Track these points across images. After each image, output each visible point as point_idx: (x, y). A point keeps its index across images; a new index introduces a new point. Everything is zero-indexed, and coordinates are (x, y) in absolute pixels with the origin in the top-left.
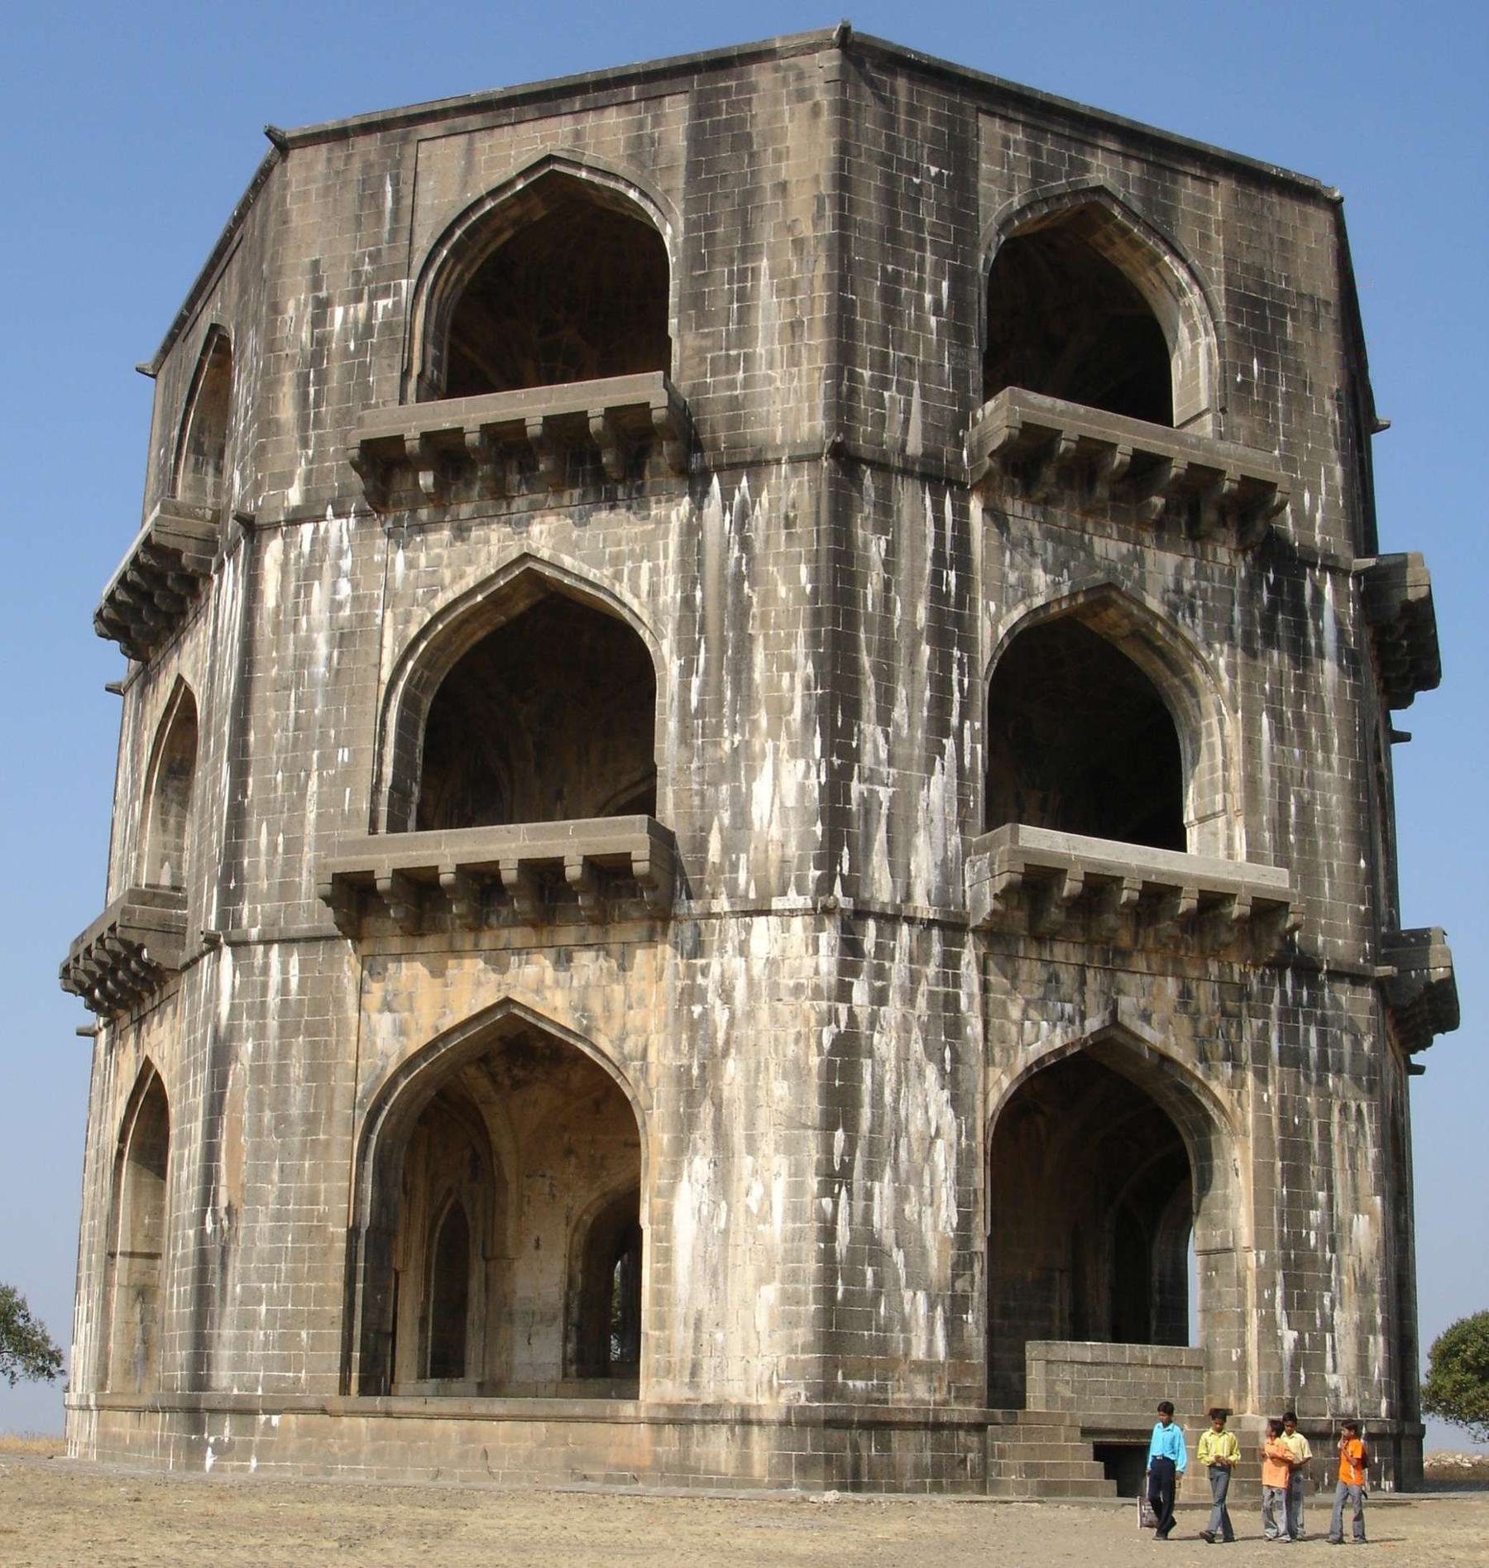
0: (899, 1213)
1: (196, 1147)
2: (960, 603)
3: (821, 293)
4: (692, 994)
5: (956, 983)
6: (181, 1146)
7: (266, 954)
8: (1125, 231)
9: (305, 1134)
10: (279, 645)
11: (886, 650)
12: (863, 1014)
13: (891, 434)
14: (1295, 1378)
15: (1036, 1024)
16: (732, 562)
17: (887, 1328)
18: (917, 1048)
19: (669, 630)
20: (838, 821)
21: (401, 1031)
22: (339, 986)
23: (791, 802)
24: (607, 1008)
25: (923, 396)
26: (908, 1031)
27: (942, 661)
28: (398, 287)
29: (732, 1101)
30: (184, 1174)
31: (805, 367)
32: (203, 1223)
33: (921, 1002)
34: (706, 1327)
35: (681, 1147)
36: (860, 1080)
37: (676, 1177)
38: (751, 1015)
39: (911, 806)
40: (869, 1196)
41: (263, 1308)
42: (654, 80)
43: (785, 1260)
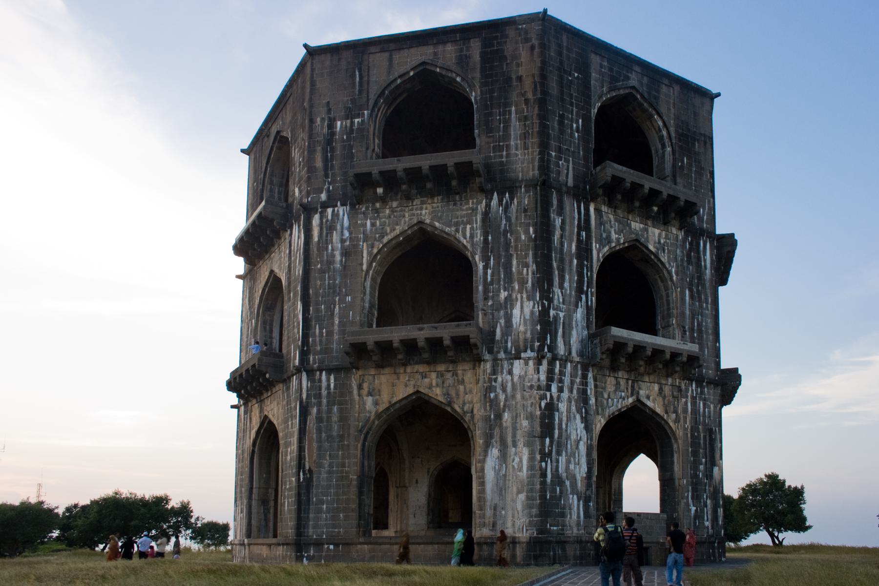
0: (567, 468)
1: (295, 447)
2: (587, 244)
3: (536, 121)
4: (490, 389)
5: (587, 385)
6: (287, 447)
7: (321, 375)
8: (641, 105)
9: (339, 442)
10: (320, 255)
11: (561, 261)
12: (555, 395)
13: (562, 178)
14: (695, 523)
15: (613, 400)
16: (503, 226)
17: (564, 508)
18: (574, 408)
20: (546, 325)
21: (376, 403)
22: (351, 387)
23: (528, 317)
24: (458, 395)
25: (573, 164)
26: (571, 402)
27: (580, 266)
28: (363, 114)
29: (506, 428)
30: (289, 458)
31: (530, 150)
32: (299, 475)
33: (575, 391)
34: (498, 509)
35: (487, 445)
36: (554, 420)
37: (486, 456)
38: (513, 397)
39: (571, 320)
40: (558, 461)
41: (325, 506)
43: (528, 485)
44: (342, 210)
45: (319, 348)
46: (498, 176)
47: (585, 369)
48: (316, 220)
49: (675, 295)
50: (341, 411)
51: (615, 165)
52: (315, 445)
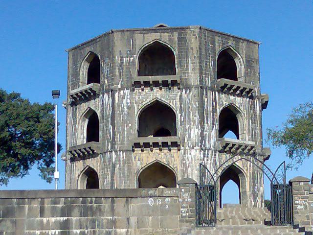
3: (198, 64)
4: (184, 159)
10: (119, 108)
11: (207, 114)
12: (206, 162)
19: (178, 110)
20: (202, 137)
21: (141, 164)
23: (196, 134)
27: (213, 115)
42: (172, 30)
45: (119, 143)
46: (185, 83)
47: (215, 152)
48: (117, 95)
51: (225, 79)
52: (118, 179)
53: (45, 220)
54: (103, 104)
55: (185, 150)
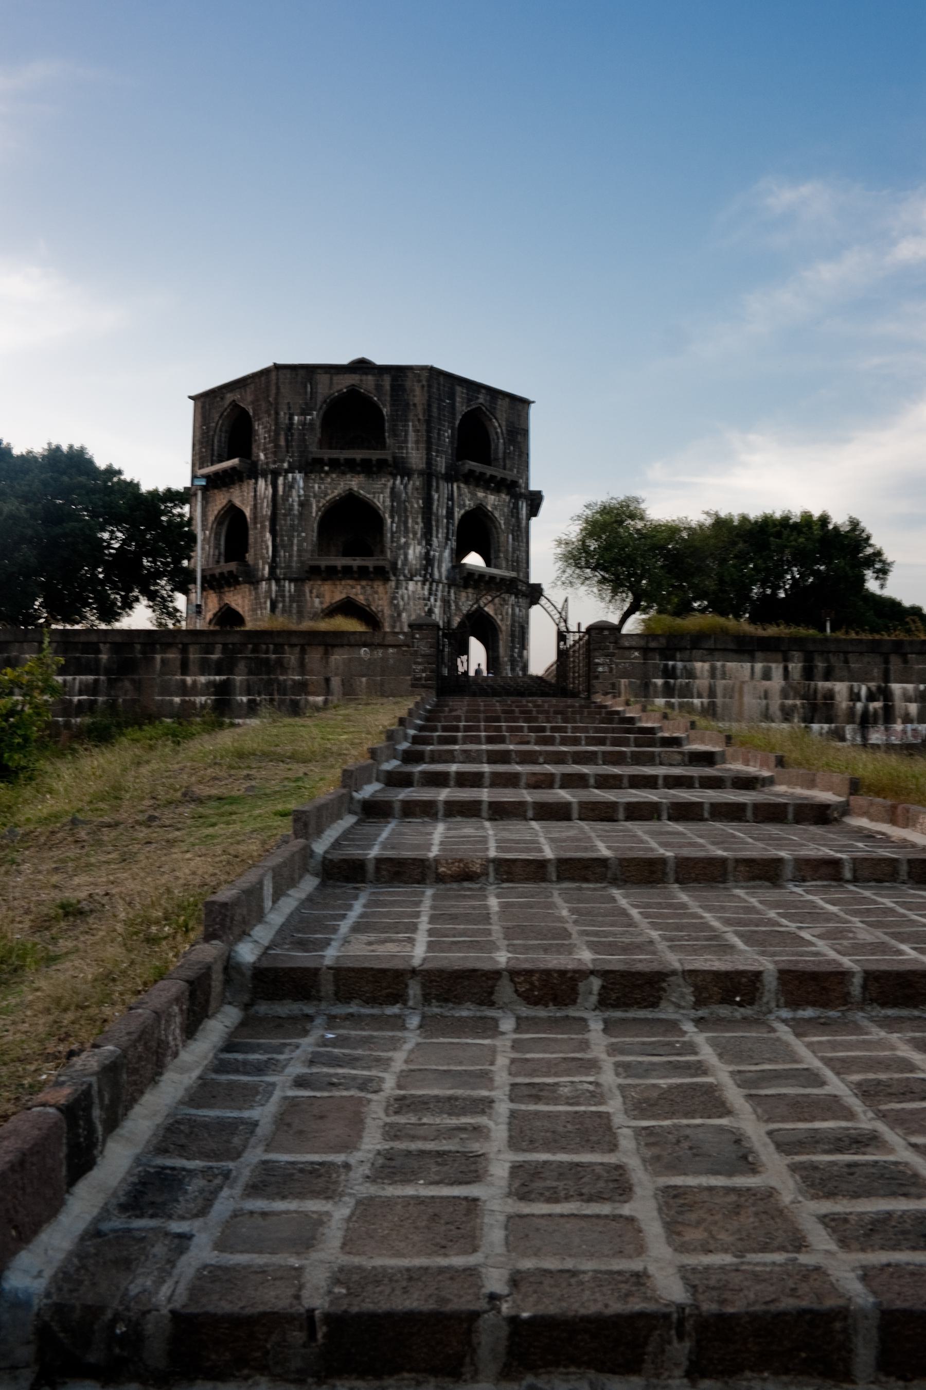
4: (394, 598)
10: (284, 504)
11: (437, 521)
20: (428, 560)
21: (321, 603)
27: (448, 523)
44: (299, 476)
47: (449, 588)
48: (281, 480)
49: (502, 538)
50: (298, 606)
53: (189, 680)
54: (255, 496)
55: (398, 581)
